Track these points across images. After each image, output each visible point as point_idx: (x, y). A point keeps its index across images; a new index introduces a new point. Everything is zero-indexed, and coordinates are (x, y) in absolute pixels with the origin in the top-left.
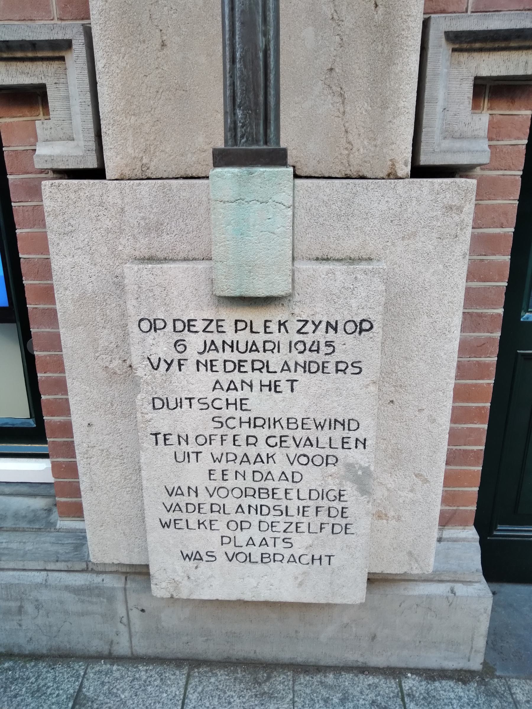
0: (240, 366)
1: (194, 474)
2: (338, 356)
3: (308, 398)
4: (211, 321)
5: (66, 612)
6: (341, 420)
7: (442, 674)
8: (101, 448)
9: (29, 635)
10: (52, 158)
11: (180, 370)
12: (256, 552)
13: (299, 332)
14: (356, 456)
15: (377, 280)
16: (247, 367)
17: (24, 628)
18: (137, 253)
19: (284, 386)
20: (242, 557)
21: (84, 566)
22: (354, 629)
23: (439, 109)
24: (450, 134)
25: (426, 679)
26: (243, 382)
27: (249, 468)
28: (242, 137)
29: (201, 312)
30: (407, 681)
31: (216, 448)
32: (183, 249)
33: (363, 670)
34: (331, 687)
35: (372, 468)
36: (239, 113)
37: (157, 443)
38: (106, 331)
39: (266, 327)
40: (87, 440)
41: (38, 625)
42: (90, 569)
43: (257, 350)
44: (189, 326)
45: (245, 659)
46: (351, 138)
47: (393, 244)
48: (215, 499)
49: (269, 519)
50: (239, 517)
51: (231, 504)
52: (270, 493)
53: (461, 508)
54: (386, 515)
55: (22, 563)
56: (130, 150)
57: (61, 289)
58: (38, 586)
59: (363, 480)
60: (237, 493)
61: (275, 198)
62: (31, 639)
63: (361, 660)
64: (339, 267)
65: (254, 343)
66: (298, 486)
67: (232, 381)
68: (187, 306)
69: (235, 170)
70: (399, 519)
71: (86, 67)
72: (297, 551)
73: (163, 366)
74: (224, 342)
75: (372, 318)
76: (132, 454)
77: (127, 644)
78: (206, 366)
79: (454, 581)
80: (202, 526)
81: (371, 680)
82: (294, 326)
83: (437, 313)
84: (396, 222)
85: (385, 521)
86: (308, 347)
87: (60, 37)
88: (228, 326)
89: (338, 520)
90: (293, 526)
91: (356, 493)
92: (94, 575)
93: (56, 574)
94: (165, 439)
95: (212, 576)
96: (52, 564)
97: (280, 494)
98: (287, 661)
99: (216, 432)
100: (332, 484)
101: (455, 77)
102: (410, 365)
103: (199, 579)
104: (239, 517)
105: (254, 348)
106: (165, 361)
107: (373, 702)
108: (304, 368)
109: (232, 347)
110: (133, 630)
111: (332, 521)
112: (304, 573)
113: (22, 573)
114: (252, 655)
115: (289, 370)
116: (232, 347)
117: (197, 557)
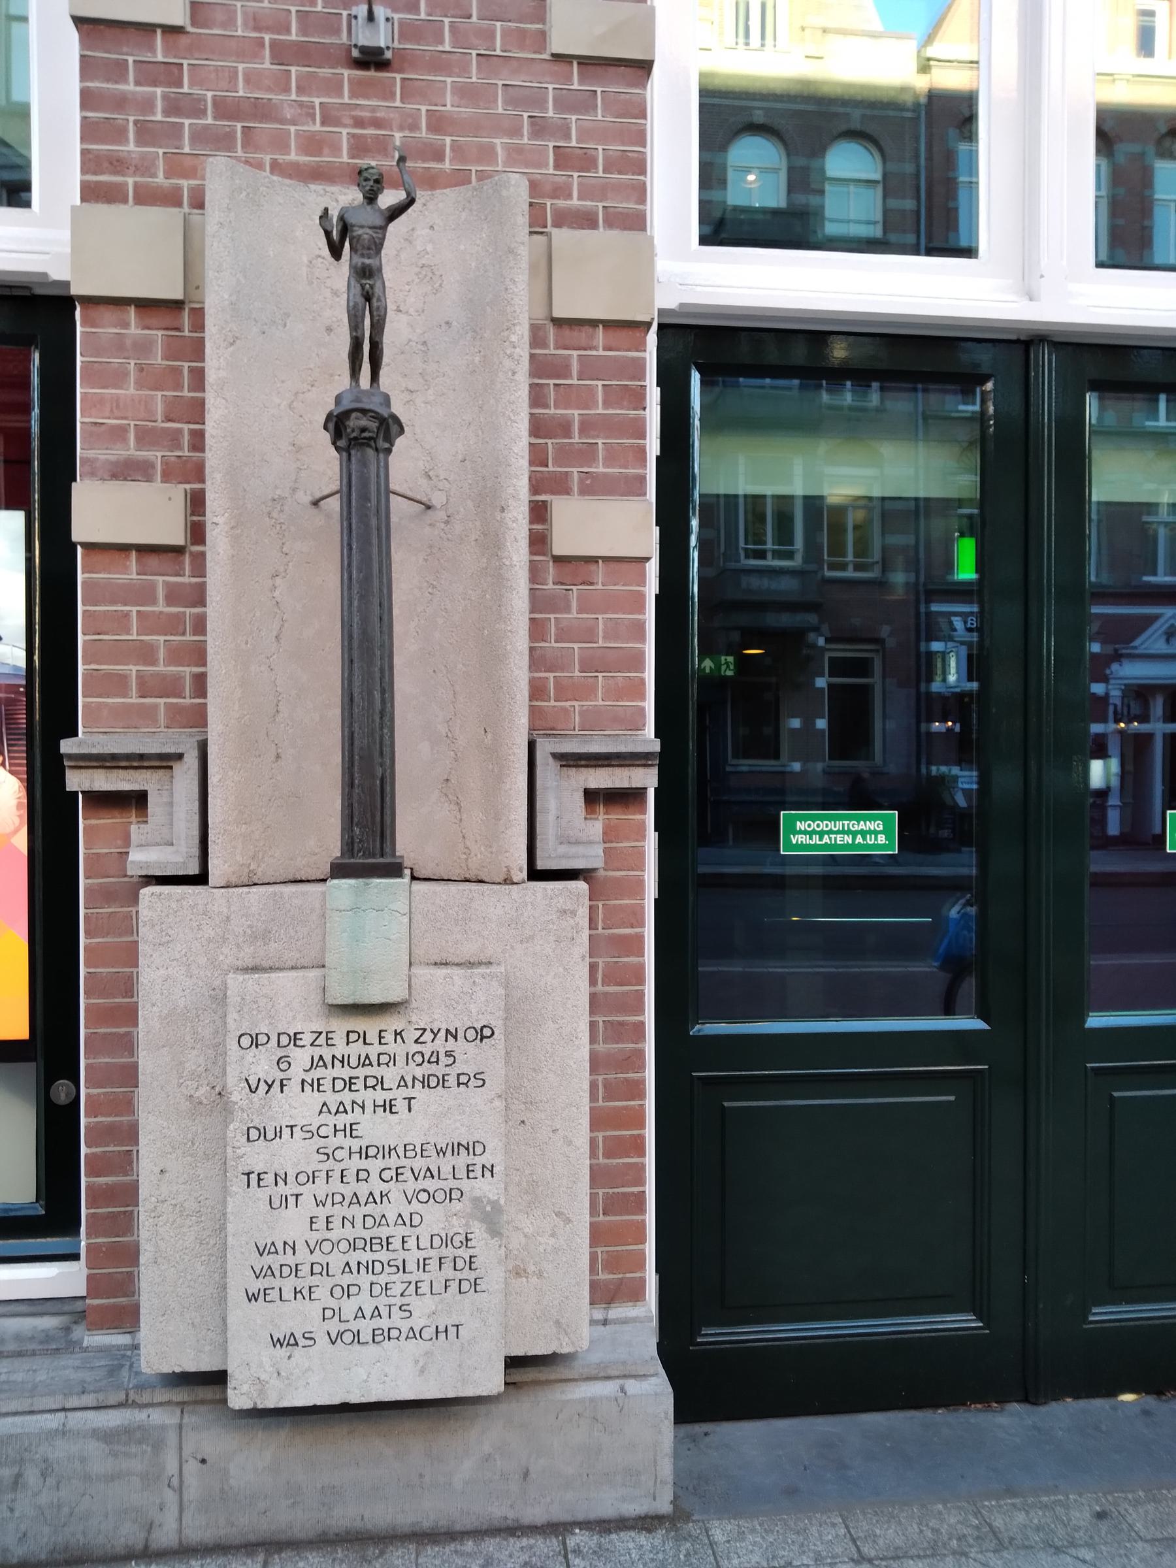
0: (351, 1084)
1: (292, 1225)
2: (459, 1068)
3: (428, 1119)
4: (321, 1033)
5: (87, 1478)
6: (464, 1143)
7: (622, 1524)
8: (173, 1202)
9: (23, 1527)
10: (148, 864)
11: (282, 1091)
12: (366, 1327)
13: (416, 1041)
14: (484, 1187)
15: (495, 984)
16: (359, 1084)
17: (17, 1514)
18: (240, 964)
19: (401, 1106)
20: (348, 1337)
21: (122, 1397)
22: (499, 1463)
23: (551, 817)
24: (565, 840)
25: (600, 1532)
26: (354, 1102)
27: (358, 1212)
28: (359, 851)
29: (308, 1024)
30: (573, 1538)
31: (321, 1188)
32: (291, 957)
33: (514, 1530)
34: (469, 1555)
35: (502, 1202)
36: (357, 830)
37: (248, 1186)
38: (195, 1052)
39: (380, 1037)
40: (158, 1192)
41: (40, 1508)
42: (130, 1401)
43: (371, 1064)
44: (295, 1039)
45: (348, 1533)
46: (468, 843)
47: (512, 947)
48: (317, 1257)
49: (382, 1279)
50: (346, 1279)
51: (336, 1261)
52: (384, 1243)
53: (628, 1275)
54: (525, 1271)
55: (30, 1400)
56: (239, 858)
57: (148, 1006)
58: (51, 1435)
59: (491, 1218)
60: (344, 1246)
61: (390, 906)
62: (25, 1535)
63: (511, 1515)
64: (457, 971)
65: (367, 1057)
66: (417, 1231)
67: (341, 1103)
68: (294, 1018)
69: (352, 881)
70: (540, 1275)
71: (196, 778)
72: (417, 1322)
73: (263, 1087)
74: (334, 1057)
75: (493, 1024)
76: (213, 1208)
77: (174, 1525)
78: (312, 1086)
79: (625, 1377)
80: (299, 1295)
81: (525, 1541)
82: (411, 1035)
83: (562, 1018)
84: (513, 926)
85: (524, 1279)
86: (426, 1058)
87: (173, 751)
88: (339, 1039)
89: (466, 1274)
90: (413, 1286)
91: (485, 1235)
92: (136, 1411)
93: (79, 1414)
94: (259, 1179)
95: (309, 1369)
96: (75, 1397)
97: (396, 1243)
98: (407, 1530)
99: (320, 1166)
100: (457, 1226)
101: (563, 794)
102: (539, 1077)
103: (292, 1374)
104: (346, 1279)
105: (367, 1062)
106: (266, 1082)
107: (526, 1563)
108: (423, 1082)
109: (342, 1062)
110: (185, 1498)
111: (459, 1275)
112: (426, 1353)
113: (28, 1418)
114: (358, 1524)
115: (406, 1086)
116: (342, 1062)
117: (290, 1341)
